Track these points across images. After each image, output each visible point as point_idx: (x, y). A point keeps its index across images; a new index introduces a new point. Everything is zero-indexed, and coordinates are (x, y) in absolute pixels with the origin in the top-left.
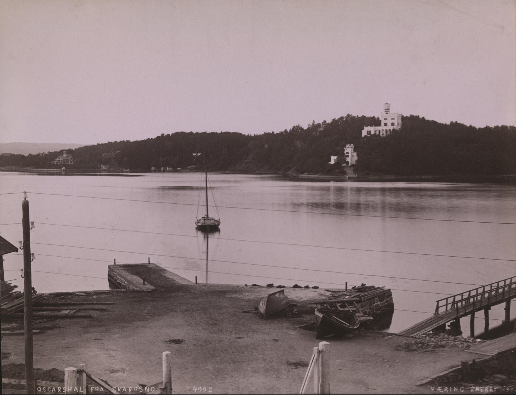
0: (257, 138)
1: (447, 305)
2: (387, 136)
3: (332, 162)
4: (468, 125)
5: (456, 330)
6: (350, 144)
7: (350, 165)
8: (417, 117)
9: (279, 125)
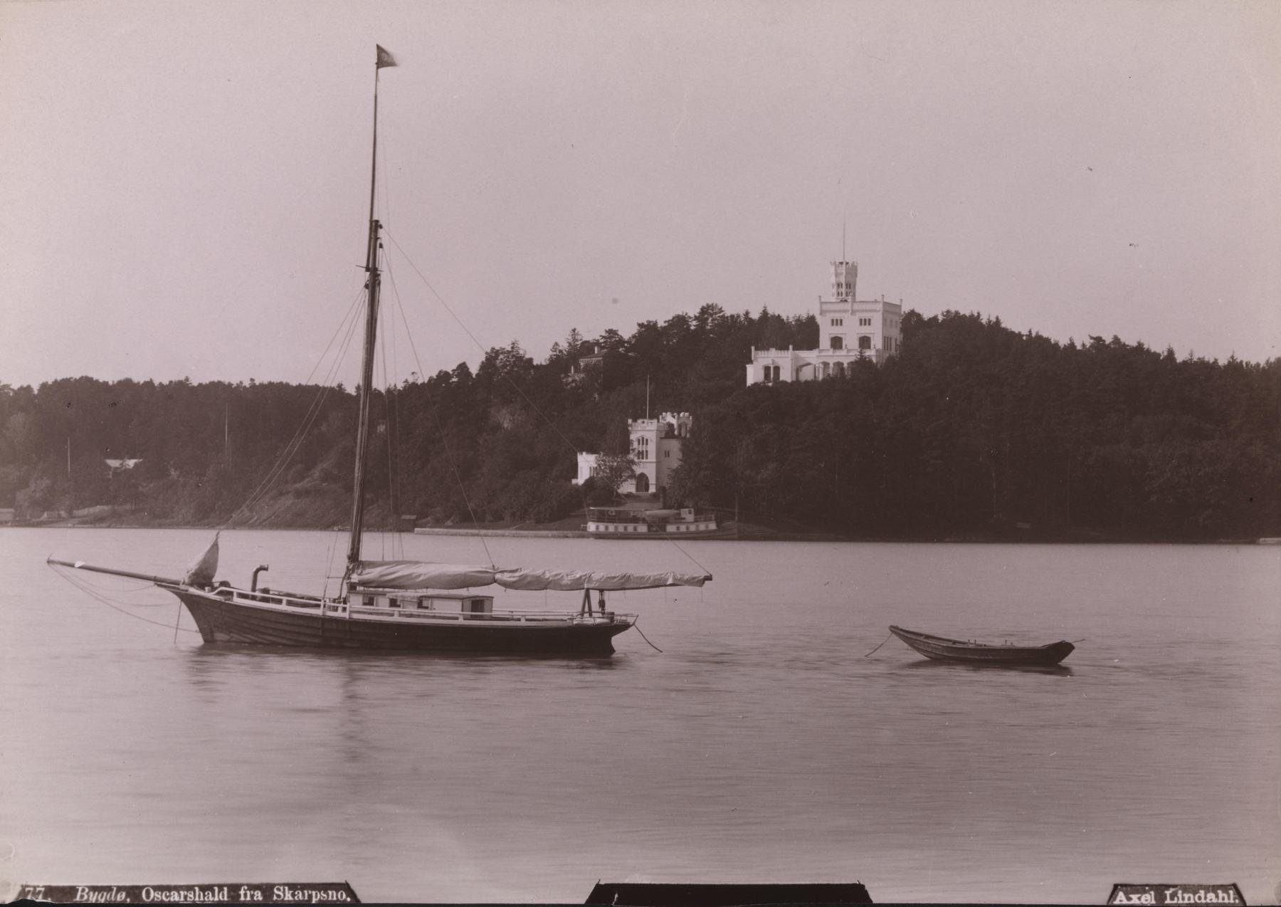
2: (829, 381)
4: (1063, 342)
7: (652, 489)
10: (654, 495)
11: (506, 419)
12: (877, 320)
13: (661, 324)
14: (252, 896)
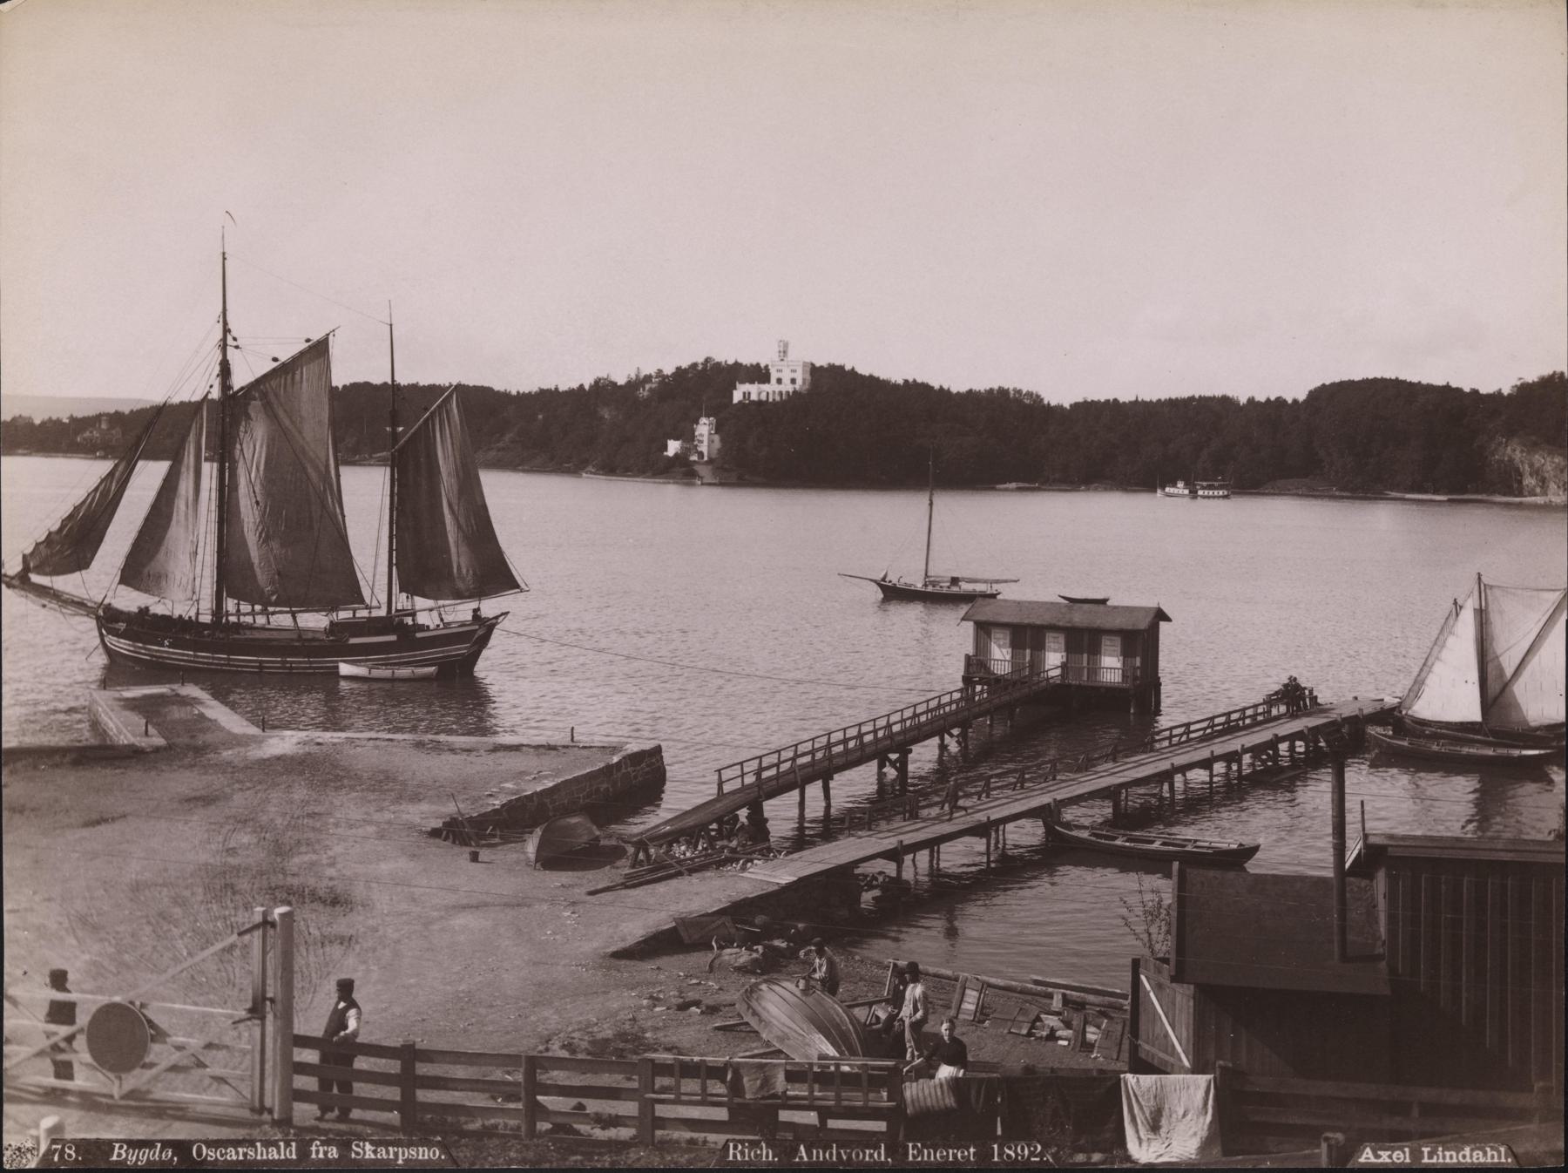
0: (522, 398)
1: (743, 775)
5: (758, 825)
6: (708, 416)
8: (842, 368)
9: (572, 375)
12: (800, 371)
13: (1506, 391)
14: (326, 1153)
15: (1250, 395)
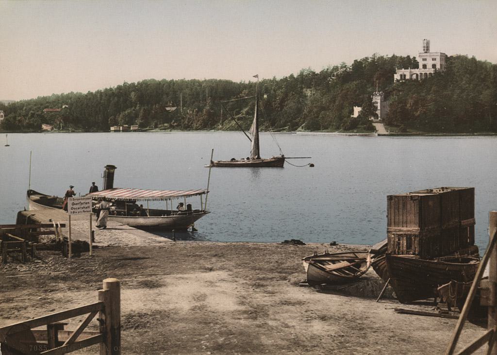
3: (356, 114)
10: (380, 120)
11: (308, 93)
12: (438, 59)
15: (105, 88)
